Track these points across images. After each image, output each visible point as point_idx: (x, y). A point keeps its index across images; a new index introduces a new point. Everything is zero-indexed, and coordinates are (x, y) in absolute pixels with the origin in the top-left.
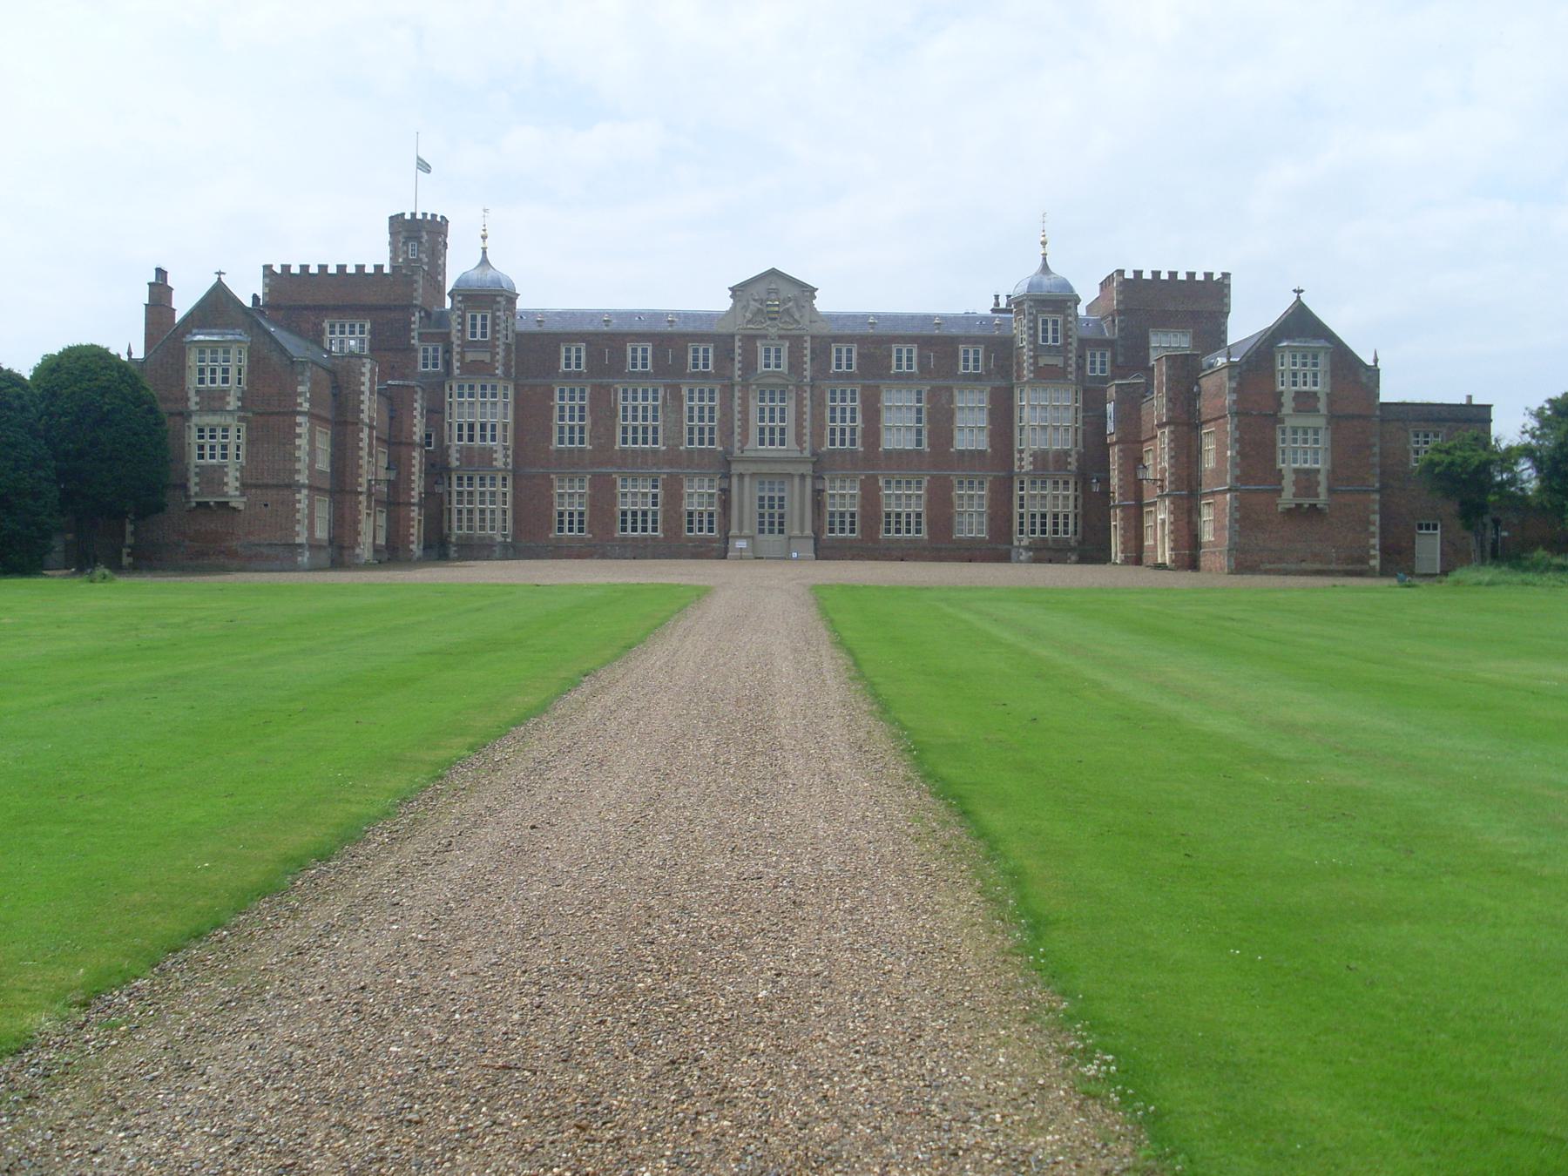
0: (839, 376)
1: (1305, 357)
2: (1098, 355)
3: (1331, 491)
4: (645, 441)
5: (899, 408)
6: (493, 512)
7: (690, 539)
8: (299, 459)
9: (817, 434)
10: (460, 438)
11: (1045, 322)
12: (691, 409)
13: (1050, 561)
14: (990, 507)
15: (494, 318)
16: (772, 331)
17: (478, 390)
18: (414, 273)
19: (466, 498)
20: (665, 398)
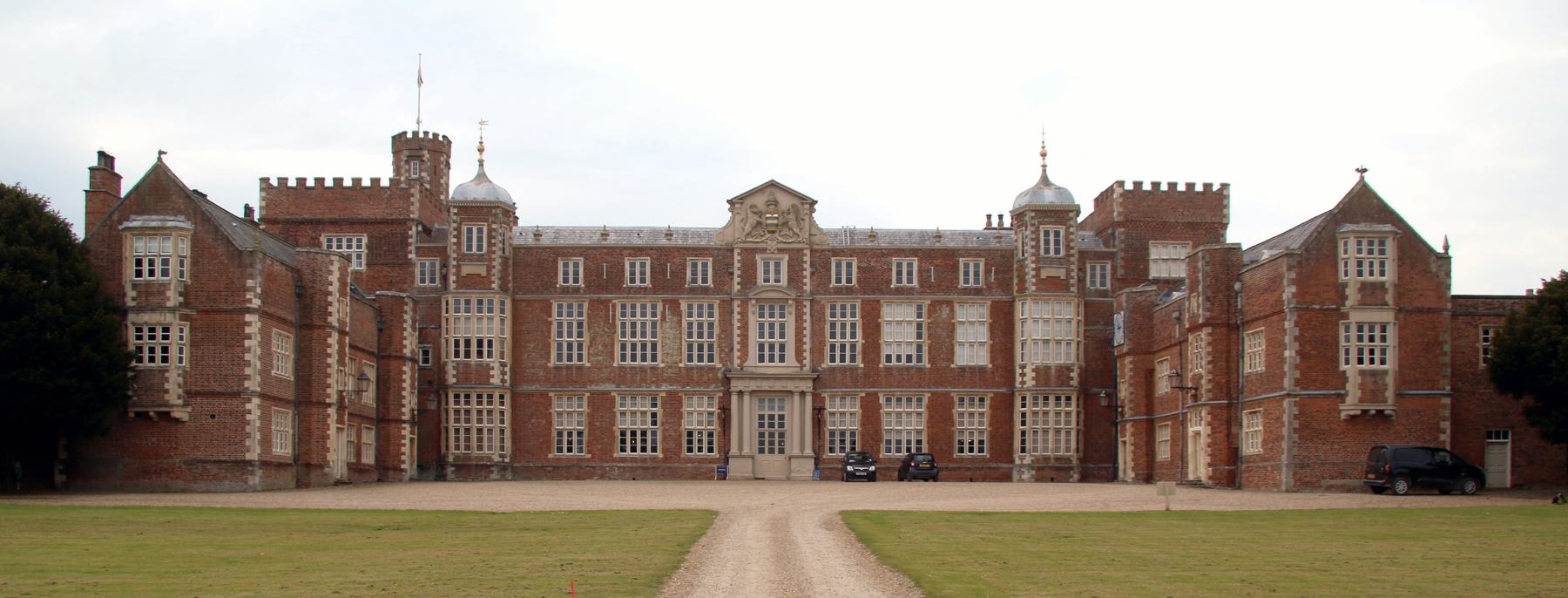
0: (838, 291)
1: (1371, 243)
2: (1098, 267)
3: (1399, 396)
4: (644, 358)
5: (899, 323)
6: (490, 431)
7: (689, 460)
8: (248, 364)
9: (817, 351)
10: (457, 354)
11: (1047, 233)
12: (690, 325)
13: (1052, 480)
14: (991, 425)
15: (490, 230)
16: (772, 245)
17: (474, 305)
18: (411, 186)
19: (463, 416)
20: (663, 314)
